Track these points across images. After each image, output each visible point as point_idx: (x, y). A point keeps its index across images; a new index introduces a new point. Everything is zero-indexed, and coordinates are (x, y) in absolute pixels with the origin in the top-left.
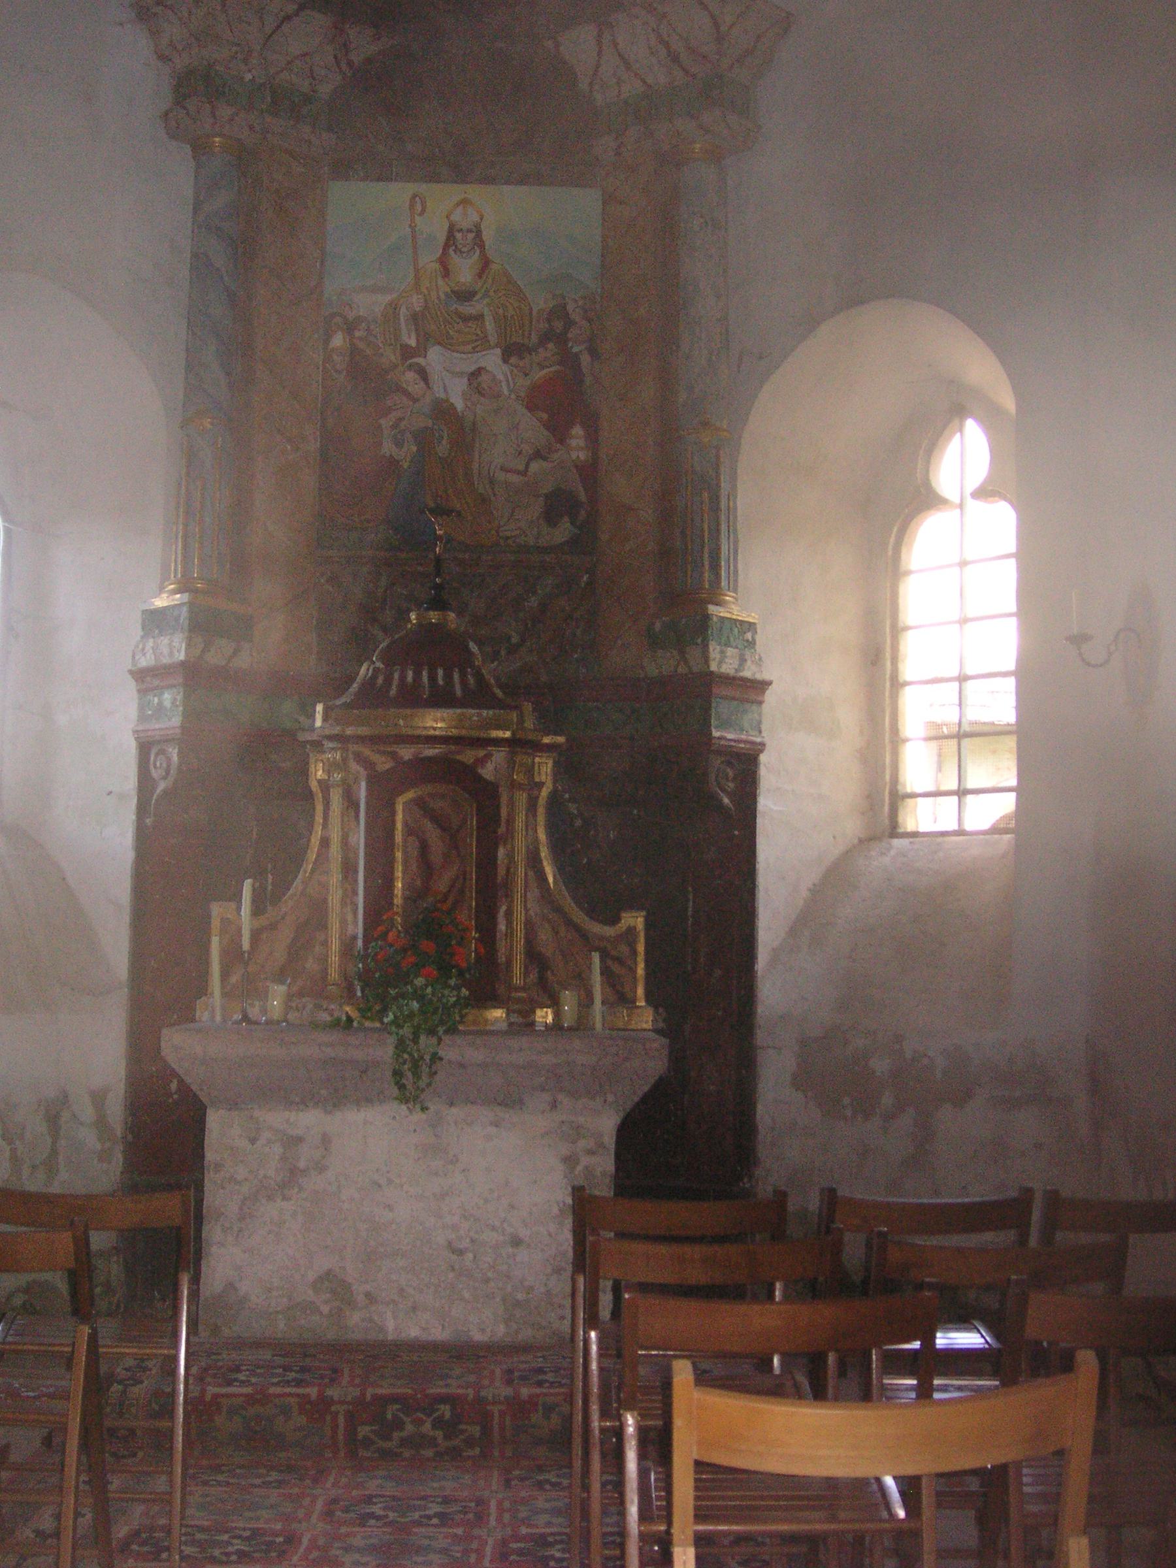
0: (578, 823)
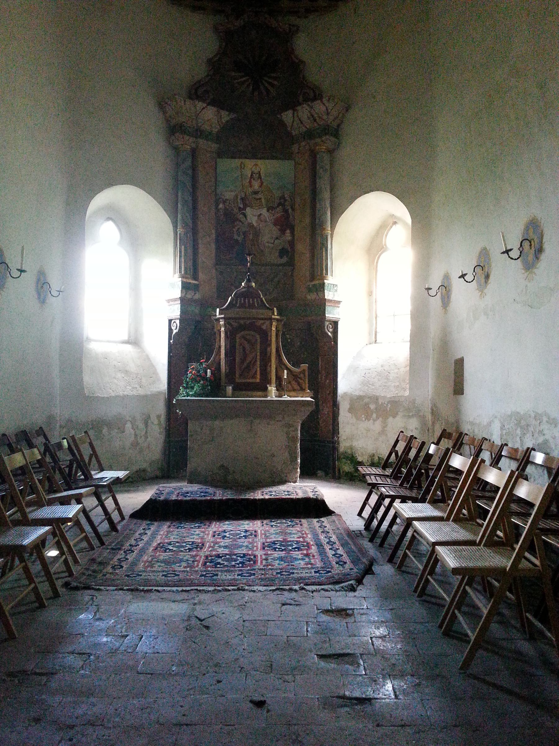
0: (289, 340)
